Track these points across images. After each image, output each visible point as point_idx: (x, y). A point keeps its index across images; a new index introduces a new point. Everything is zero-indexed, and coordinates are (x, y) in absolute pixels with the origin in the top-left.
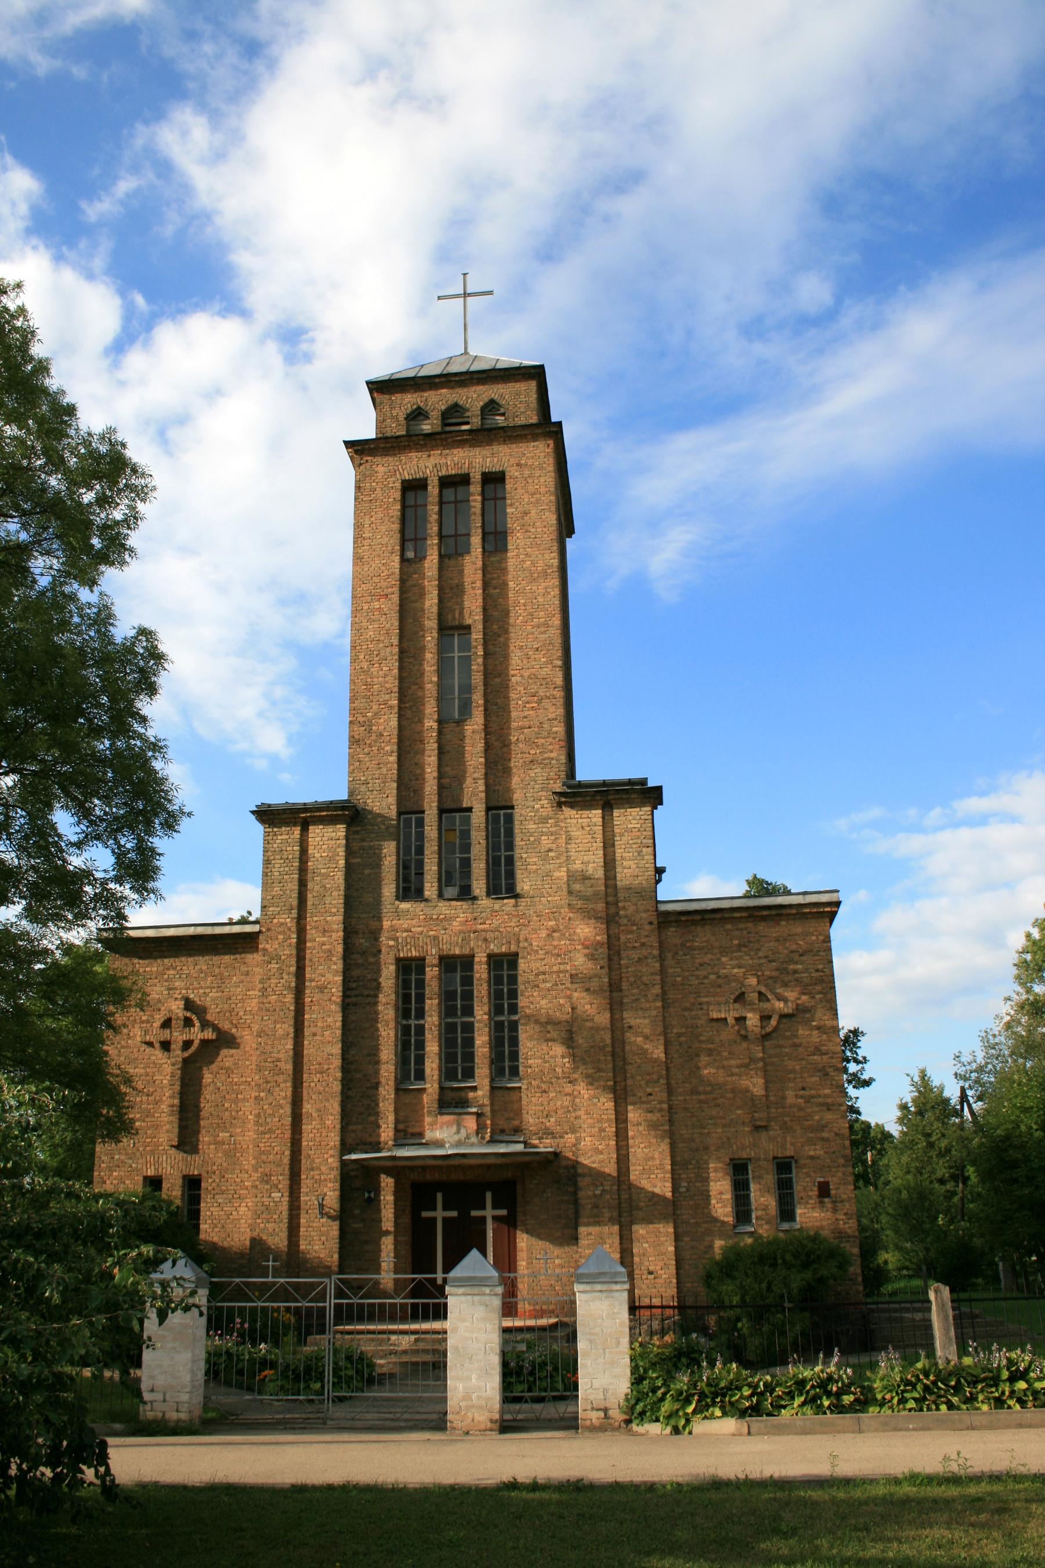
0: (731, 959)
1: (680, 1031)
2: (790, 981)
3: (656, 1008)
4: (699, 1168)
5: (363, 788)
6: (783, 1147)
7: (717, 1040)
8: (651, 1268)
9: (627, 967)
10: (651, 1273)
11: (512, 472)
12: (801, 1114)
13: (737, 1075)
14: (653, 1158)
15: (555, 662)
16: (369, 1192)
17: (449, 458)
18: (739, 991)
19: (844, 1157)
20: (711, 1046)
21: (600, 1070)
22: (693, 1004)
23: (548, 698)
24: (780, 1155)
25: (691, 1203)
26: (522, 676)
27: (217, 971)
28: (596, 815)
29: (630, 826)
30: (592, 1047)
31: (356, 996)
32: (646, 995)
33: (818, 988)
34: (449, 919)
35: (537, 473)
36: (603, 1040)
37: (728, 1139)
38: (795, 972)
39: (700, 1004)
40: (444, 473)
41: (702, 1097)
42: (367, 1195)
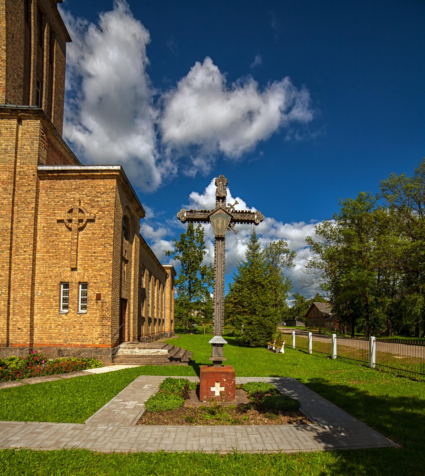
0: (71, 195)
1: (44, 225)
2: (95, 205)
3: (32, 213)
6: (83, 277)
8: (20, 327)
9: (21, 194)
10: (19, 329)
12: (92, 264)
13: (67, 245)
14: (24, 280)
15: (2, 47)
18: (71, 208)
20: (57, 232)
21: (5, 240)
22: (51, 214)
24: (81, 281)
25: (42, 300)
28: (14, 122)
29: (30, 130)
32: (28, 208)
33: (107, 209)
36: (7, 226)
37: (60, 273)
38: (98, 201)
39: (54, 214)
41: (51, 254)
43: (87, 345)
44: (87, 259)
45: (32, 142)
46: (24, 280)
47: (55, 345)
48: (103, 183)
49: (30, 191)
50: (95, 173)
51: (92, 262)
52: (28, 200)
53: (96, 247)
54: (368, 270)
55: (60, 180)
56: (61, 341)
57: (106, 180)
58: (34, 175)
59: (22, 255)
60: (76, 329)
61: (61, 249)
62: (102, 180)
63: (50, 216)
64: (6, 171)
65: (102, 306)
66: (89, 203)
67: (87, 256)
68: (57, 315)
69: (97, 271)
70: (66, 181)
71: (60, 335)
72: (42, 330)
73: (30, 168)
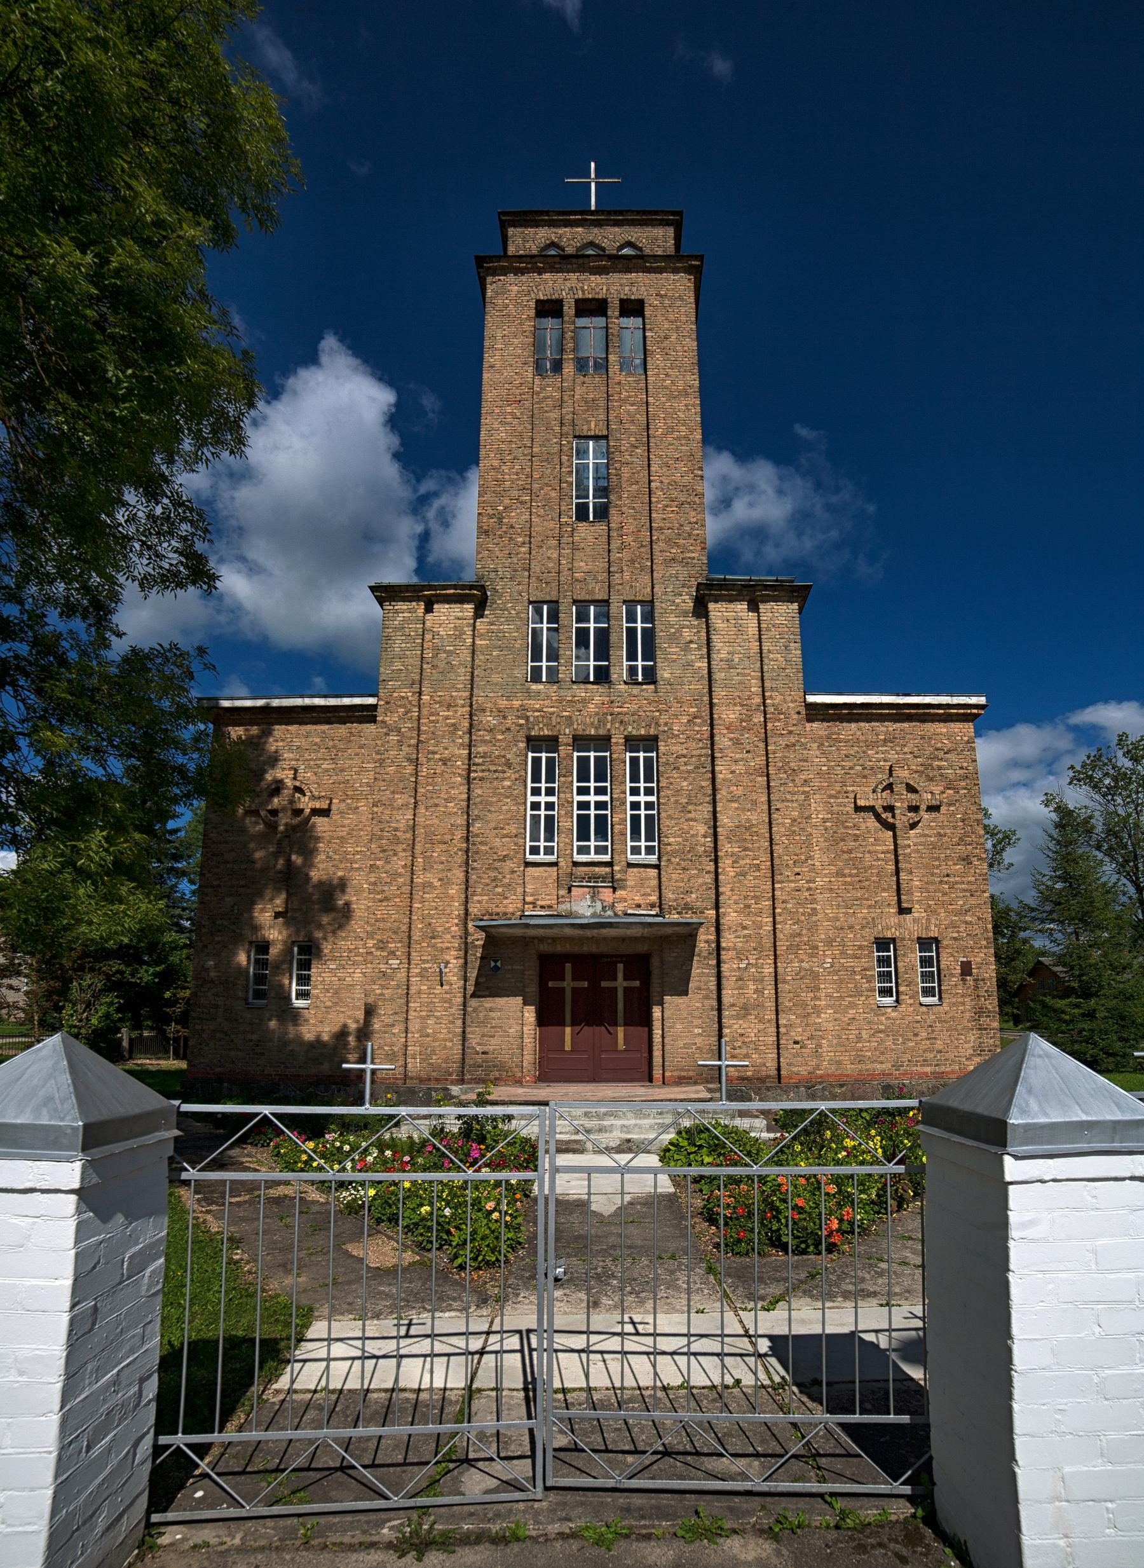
0: (877, 753)
4: (844, 946)
5: (493, 575)
6: (927, 928)
7: (863, 827)
8: (798, 1038)
10: (796, 1043)
11: (652, 302)
12: (945, 898)
14: (800, 935)
16: (496, 961)
17: (586, 283)
19: (987, 939)
23: (689, 503)
26: (661, 482)
27: (331, 743)
30: (737, 827)
31: (483, 771)
32: (793, 781)
33: (963, 784)
34: (584, 701)
35: (679, 303)
38: (940, 768)
40: (580, 295)
41: (848, 879)
42: (493, 964)
43: (947, 1072)
44: (932, 888)
45: (786, 647)
46: (800, 935)
47: (873, 1076)
48: (945, 730)
49: (794, 745)
50: (932, 711)
51: (945, 894)
52: (792, 764)
53: (950, 863)
54: (118, 827)
55: (849, 721)
56: (886, 1066)
57: (952, 725)
58: (799, 713)
59: (791, 881)
60: (919, 1038)
61: (871, 867)
62: (942, 725)
63: (837, 798)
64: (735, 705)
65: (976, 988)
66: (922, 772)
67: (932, 883)
68: (872, 1010)
69: (958, 913)
70: (862, 724)
71: (882, 1053)
72: (839, 1044)
73: (789, 699)
